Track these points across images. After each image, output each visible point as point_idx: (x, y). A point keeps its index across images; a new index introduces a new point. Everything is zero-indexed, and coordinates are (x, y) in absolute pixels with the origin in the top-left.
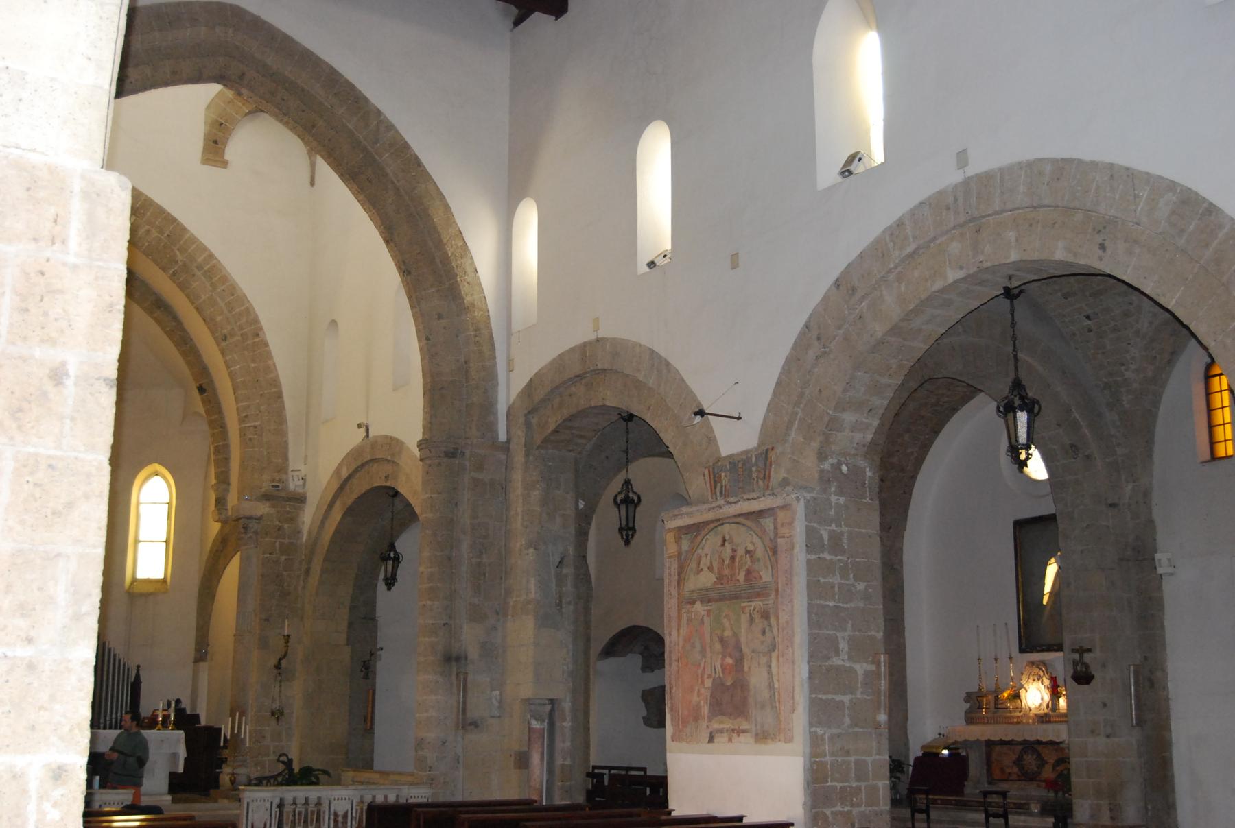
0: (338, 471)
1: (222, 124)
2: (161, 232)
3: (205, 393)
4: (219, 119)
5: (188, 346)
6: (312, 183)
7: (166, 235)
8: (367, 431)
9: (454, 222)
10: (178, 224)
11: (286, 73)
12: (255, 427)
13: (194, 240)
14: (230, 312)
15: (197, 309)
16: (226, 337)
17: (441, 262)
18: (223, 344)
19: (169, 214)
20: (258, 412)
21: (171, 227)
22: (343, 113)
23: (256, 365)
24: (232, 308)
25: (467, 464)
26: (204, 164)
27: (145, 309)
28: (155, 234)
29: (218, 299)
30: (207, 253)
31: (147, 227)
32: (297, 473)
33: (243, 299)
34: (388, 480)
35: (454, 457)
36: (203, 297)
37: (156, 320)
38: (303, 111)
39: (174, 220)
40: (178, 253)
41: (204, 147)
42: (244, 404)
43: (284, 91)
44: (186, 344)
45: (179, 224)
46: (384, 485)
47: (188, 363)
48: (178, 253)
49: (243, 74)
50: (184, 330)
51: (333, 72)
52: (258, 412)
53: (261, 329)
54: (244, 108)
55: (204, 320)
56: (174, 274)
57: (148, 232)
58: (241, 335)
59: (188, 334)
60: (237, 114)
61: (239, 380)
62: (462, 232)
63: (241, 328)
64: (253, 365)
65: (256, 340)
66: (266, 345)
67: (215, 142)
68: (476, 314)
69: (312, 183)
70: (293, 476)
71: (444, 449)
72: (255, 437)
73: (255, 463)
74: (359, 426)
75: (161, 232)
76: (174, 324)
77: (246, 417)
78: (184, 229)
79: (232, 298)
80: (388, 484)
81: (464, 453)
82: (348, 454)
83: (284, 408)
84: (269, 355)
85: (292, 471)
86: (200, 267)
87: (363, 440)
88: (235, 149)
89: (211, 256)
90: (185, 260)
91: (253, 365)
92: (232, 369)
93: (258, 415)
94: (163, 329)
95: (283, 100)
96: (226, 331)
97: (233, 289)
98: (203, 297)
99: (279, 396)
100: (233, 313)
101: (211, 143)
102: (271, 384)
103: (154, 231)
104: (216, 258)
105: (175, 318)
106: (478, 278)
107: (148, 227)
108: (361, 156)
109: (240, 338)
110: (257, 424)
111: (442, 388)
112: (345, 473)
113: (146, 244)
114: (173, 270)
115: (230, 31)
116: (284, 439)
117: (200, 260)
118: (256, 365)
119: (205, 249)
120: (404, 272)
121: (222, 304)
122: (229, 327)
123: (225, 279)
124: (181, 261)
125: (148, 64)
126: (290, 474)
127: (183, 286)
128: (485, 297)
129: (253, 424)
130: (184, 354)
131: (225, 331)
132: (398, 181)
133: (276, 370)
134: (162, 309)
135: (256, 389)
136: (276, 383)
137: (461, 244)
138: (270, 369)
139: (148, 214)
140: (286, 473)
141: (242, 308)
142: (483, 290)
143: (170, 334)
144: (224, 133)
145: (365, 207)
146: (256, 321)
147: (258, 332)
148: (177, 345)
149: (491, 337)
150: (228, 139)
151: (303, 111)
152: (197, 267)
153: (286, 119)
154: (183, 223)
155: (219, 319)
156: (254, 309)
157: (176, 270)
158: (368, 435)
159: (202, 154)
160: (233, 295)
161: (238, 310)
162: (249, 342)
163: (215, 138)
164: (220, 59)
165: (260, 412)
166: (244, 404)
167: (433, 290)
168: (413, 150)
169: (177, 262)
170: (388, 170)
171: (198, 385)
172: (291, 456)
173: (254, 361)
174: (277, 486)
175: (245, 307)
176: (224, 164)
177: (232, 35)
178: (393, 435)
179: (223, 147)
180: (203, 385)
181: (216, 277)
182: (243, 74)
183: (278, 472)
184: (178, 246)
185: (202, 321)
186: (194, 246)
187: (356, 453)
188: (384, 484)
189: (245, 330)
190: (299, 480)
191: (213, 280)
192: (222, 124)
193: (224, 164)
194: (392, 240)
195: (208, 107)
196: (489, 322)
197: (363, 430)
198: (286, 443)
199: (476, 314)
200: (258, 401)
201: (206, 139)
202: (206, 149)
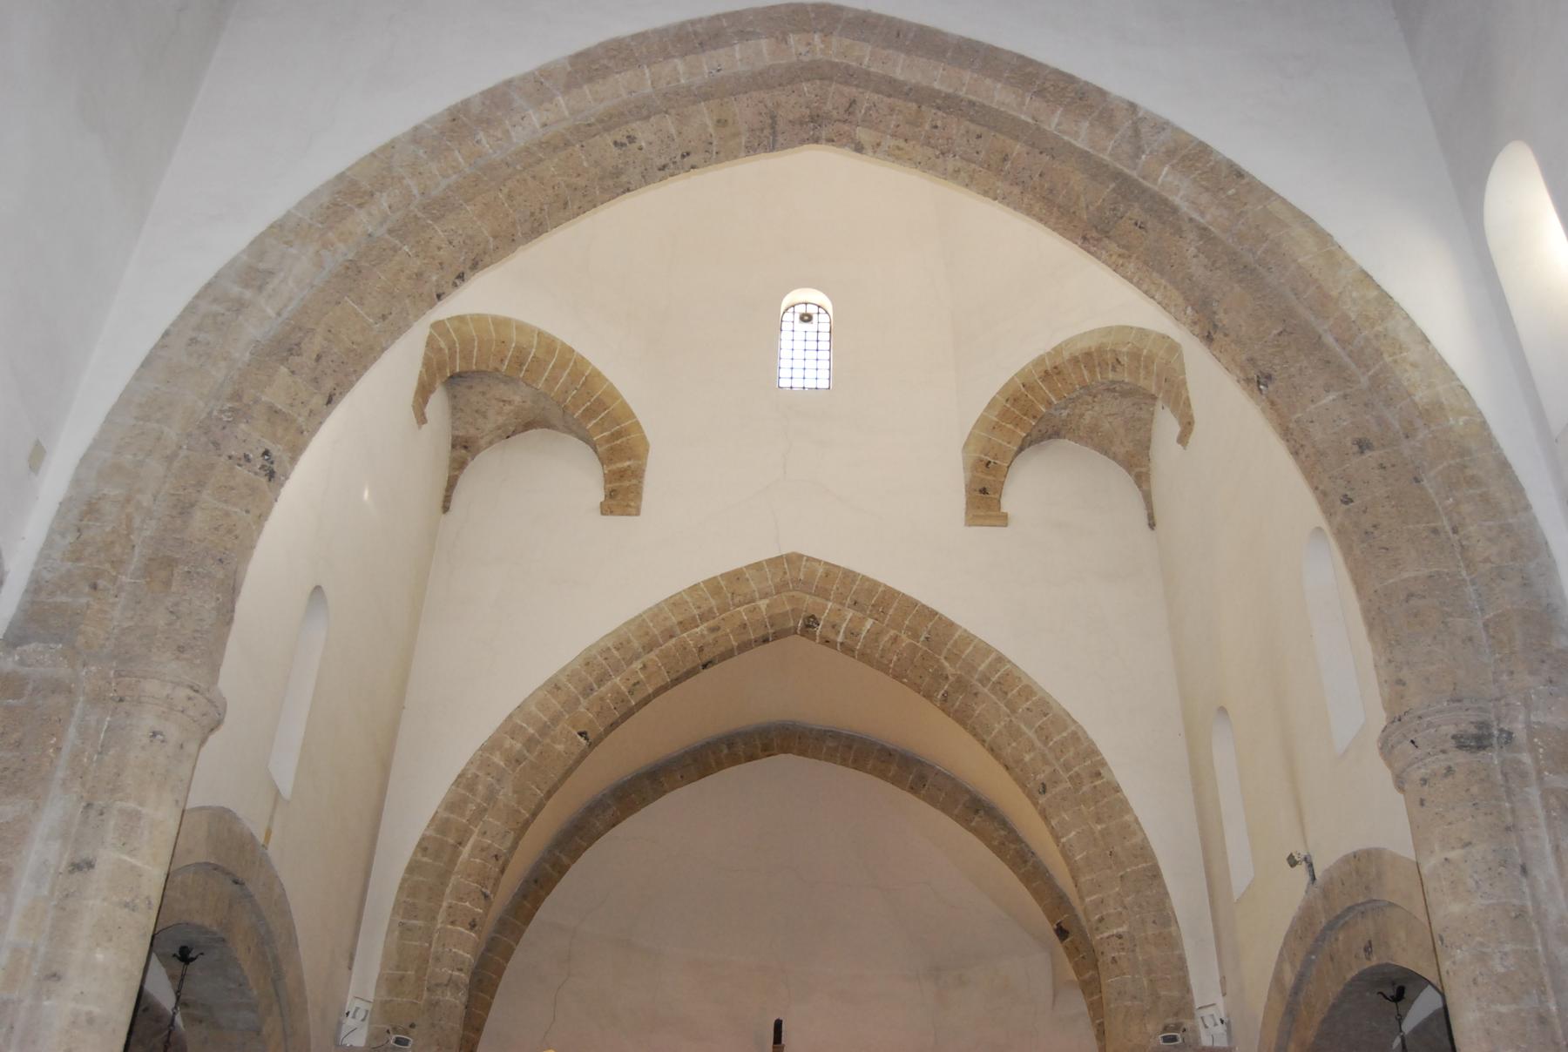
0: (1278, 978)
1: (990, 462)
2: (916, 636)
3: (1067, 937)
4: (983, 456)
5: (1029, 864)
6: (1152, 525)
7: (922, 639)
8: (1310, 865)
9: (1347, 258)
10: (940, 618)
11: (936, 85)
12: (1120, 937)
13: (969, 638)
14: (1045, 743)
15: (991, 750)
16: (1044, 786)
17: (1337, 340)
18: (1042, 800)
19: (923, 606)
20: (1120, 909)
21: (930, 624)
22: (1059, 124)
23: (1104, 826)
24: (1047, 738)
25: (1526, 758)
26: (970, 525)
27: (957, 818)
28: (905, 640)
29: (1023, 726)
30: (993, 656)
31: (892, 632)
32: (1211, 1011)
33: (1062, 720)
34: (1370, 953)
35: (1481, 747)
36: (997, 727)
37: (975, 831)
38: (979, 137)
39: (933, 613)
40: (946, 664)
41: (967, 503)
42: (1094, 897)
43: (934, 111)
44: (1025, 862)
45: (941, 618)
46: (1366, 967)
47: (1036, 894)
48: (946, 664)
49: (853, 102)
50: (1018, 839)
51: (1026, 62)
52: (1120, 909)
53: (1103, 763)
54: (1018, 431)
55: (1007, 767)
56: (945, 698)
57: (895, 639)
58: (1070, 778)
59: (1027, 846)
60: (1009, 443)
61: (1078, 858)
62: (1370, 273)
63: (1067, 767)
64: (1099, 827)
65: (1098, 783)
66: (1117, 789)
67: (984, 491)
68: (1452, 422)
69: (1152, 525)
70: (1202, 1018)
71: (1452, 730)
72: (1123, 954)
73: (1128, 1003)
74: (1292, 862)
75: (916, 636)
76: (1003, 833)
77: (1101, 920)
78: (951, 625)
79: (1045, 719)
80: (1375, 961)
81: (1510, 734)
82: (1287, 936)
83: (1167, 894)
84: (1124, 806)
85: (1200, 1008)
86: (984, 679)
87: (1306, 892)
88: (1012, 500)
89: (1001, 659)
90: (959, 673)
91: (1099, 827)
92: (1063, 840)
93: (1121, 913)
94: (989, 845)
95: (936, 127)
96: (1043, 775)
97: (1044, 706)
98: (997, 727)
99: (1155, 874)
100: (1051, 744)
101: (977, 494)
102: (1136, 857)
103: (904, 636)
104: (1009, 662)
105: (1004, 823)
106: (1435, 351)
107: (895, 632)
108: (1112, 185)
109: (1069, 785)
110: (1120, 930)
111: (1411, 595)
112: (1289, 978)
113: (895, 658)
114: (942, 692)
115: (817, 38)
116: (1177, 952)
117: (982, 667)
118: (1104, 826)
119: (988, 650)
120: (1259, 383)
121: (1031, 734)
122: (1048, 770)
123: (1028, 691)
124: (953, 675)
125: (666, 112)
126: (1198, 1014)
127: (962, 718)
128: (1463, 387)
129: (1115, 931)
130: (1026, 879)
131: (1041, 777)
132: (1202, 214)
133: (1141, 829)
134: (982, 813)
135: (1110, 868)
136: (1144, 852)
137: (1375, 293)
138: (1131, 828)
139: (891, 612)
140: (1192, 1016)
141: (1065, 734)
142: (1453, 373)
143: (999, 851)
144: (994, 476)
145: (1145, 287)
146: (1093, 751)
147: (1098, 769)
148: (1013, 866)
149: (1504, 466)
150: (1003, 483)
151: (979, 137)
152: (980, 681)
153: (951, 163)
154: (947, 615)
155: (1027, 758)
156: (1085, 732)
157: (946, 692)
158: (1314, 878)
159: (966, 513)
160: (1045, 715)
161: (1057, 738)
162: (1085, 788)
163: (981, 487)
164: (805, 87)
165: (1125, 908)
166: (1094, 897)
167: (1332, 396)
168: (1219, 153)
169: (947, 678)
170: (1176, 200)
171: (1055, 927)
172: (1194, 981)
173: (1099, 820)
174: (1174, 1039)
175: (1069, 731)
176: (1003, 520)
177: (822, 46)
178: (1356, 848)
179: (997, 496)
180: (1062, 925)
181: (1012, 690)
182: (853, 102)
183: (1176, 1014)
184: (945, 652)
185: (1002, 769)
186: (971, 648)
187: (1305, 918)
188: (1367, 965)
189: (1076, 769)
190: (1216, 1025)
191: (1009, 696)
192: (990, 462)
193: (1003, 520)
194: (1215, 326)
195: (966, 445)
196: (1490, 434)
197: (1302, 869)
198: (1182, 959)
199: (1452, 422)
200: (1117, 889)
201: (969, 490)
202: (971, 504)
